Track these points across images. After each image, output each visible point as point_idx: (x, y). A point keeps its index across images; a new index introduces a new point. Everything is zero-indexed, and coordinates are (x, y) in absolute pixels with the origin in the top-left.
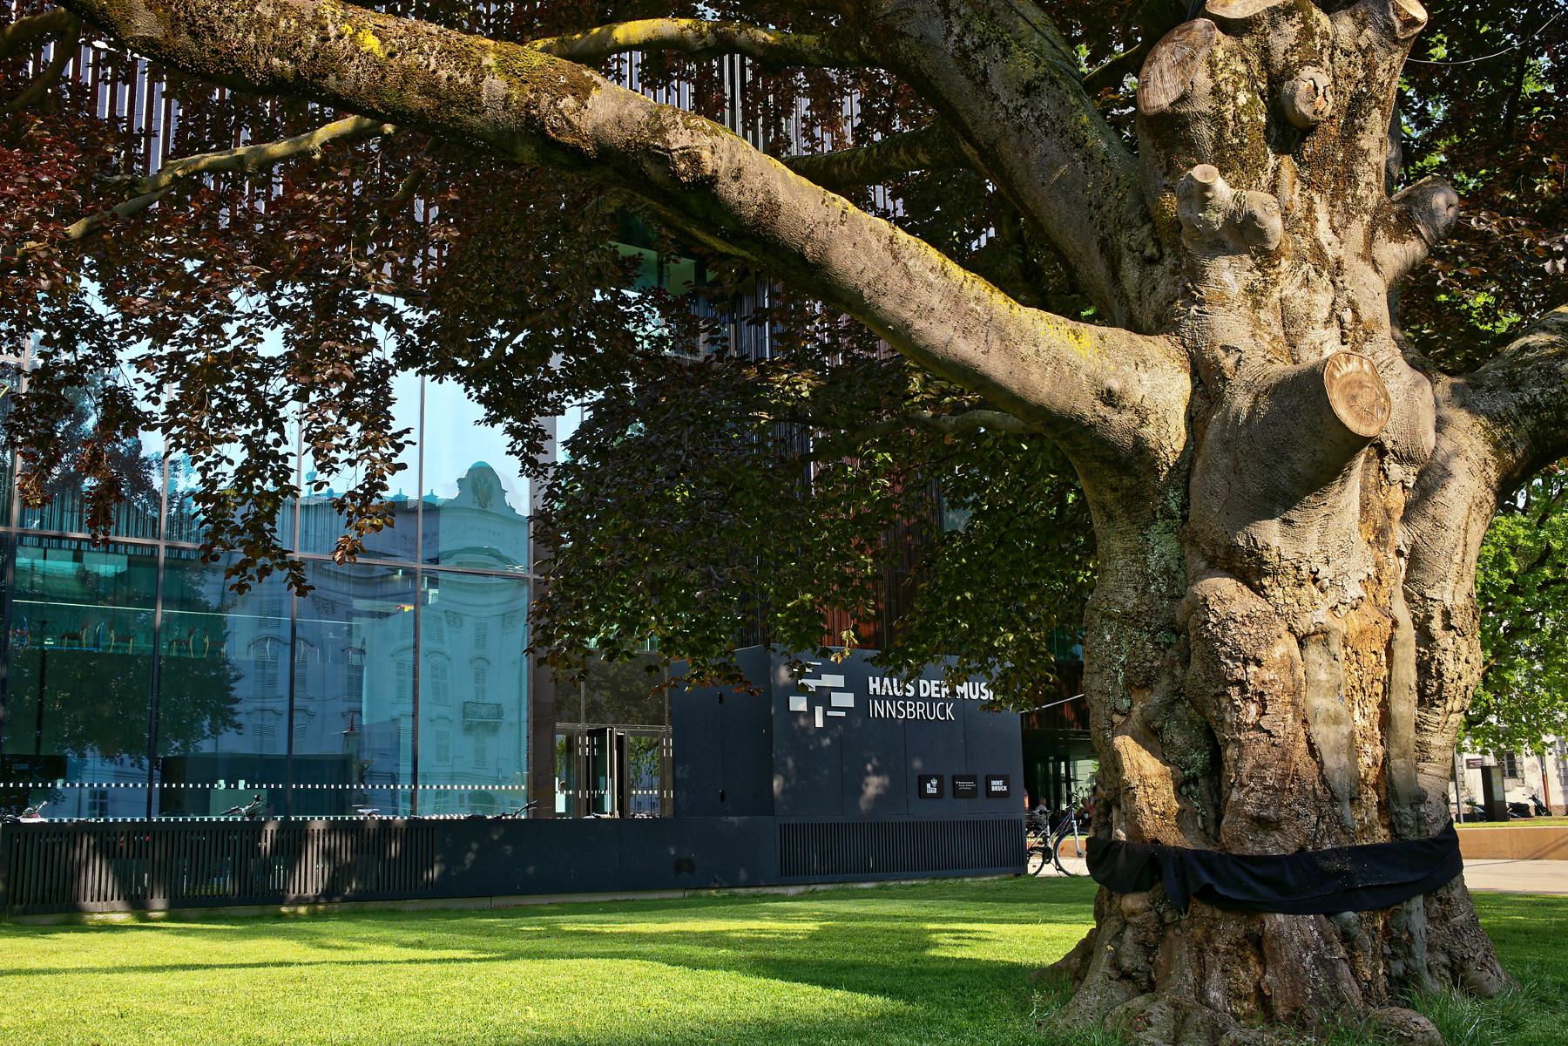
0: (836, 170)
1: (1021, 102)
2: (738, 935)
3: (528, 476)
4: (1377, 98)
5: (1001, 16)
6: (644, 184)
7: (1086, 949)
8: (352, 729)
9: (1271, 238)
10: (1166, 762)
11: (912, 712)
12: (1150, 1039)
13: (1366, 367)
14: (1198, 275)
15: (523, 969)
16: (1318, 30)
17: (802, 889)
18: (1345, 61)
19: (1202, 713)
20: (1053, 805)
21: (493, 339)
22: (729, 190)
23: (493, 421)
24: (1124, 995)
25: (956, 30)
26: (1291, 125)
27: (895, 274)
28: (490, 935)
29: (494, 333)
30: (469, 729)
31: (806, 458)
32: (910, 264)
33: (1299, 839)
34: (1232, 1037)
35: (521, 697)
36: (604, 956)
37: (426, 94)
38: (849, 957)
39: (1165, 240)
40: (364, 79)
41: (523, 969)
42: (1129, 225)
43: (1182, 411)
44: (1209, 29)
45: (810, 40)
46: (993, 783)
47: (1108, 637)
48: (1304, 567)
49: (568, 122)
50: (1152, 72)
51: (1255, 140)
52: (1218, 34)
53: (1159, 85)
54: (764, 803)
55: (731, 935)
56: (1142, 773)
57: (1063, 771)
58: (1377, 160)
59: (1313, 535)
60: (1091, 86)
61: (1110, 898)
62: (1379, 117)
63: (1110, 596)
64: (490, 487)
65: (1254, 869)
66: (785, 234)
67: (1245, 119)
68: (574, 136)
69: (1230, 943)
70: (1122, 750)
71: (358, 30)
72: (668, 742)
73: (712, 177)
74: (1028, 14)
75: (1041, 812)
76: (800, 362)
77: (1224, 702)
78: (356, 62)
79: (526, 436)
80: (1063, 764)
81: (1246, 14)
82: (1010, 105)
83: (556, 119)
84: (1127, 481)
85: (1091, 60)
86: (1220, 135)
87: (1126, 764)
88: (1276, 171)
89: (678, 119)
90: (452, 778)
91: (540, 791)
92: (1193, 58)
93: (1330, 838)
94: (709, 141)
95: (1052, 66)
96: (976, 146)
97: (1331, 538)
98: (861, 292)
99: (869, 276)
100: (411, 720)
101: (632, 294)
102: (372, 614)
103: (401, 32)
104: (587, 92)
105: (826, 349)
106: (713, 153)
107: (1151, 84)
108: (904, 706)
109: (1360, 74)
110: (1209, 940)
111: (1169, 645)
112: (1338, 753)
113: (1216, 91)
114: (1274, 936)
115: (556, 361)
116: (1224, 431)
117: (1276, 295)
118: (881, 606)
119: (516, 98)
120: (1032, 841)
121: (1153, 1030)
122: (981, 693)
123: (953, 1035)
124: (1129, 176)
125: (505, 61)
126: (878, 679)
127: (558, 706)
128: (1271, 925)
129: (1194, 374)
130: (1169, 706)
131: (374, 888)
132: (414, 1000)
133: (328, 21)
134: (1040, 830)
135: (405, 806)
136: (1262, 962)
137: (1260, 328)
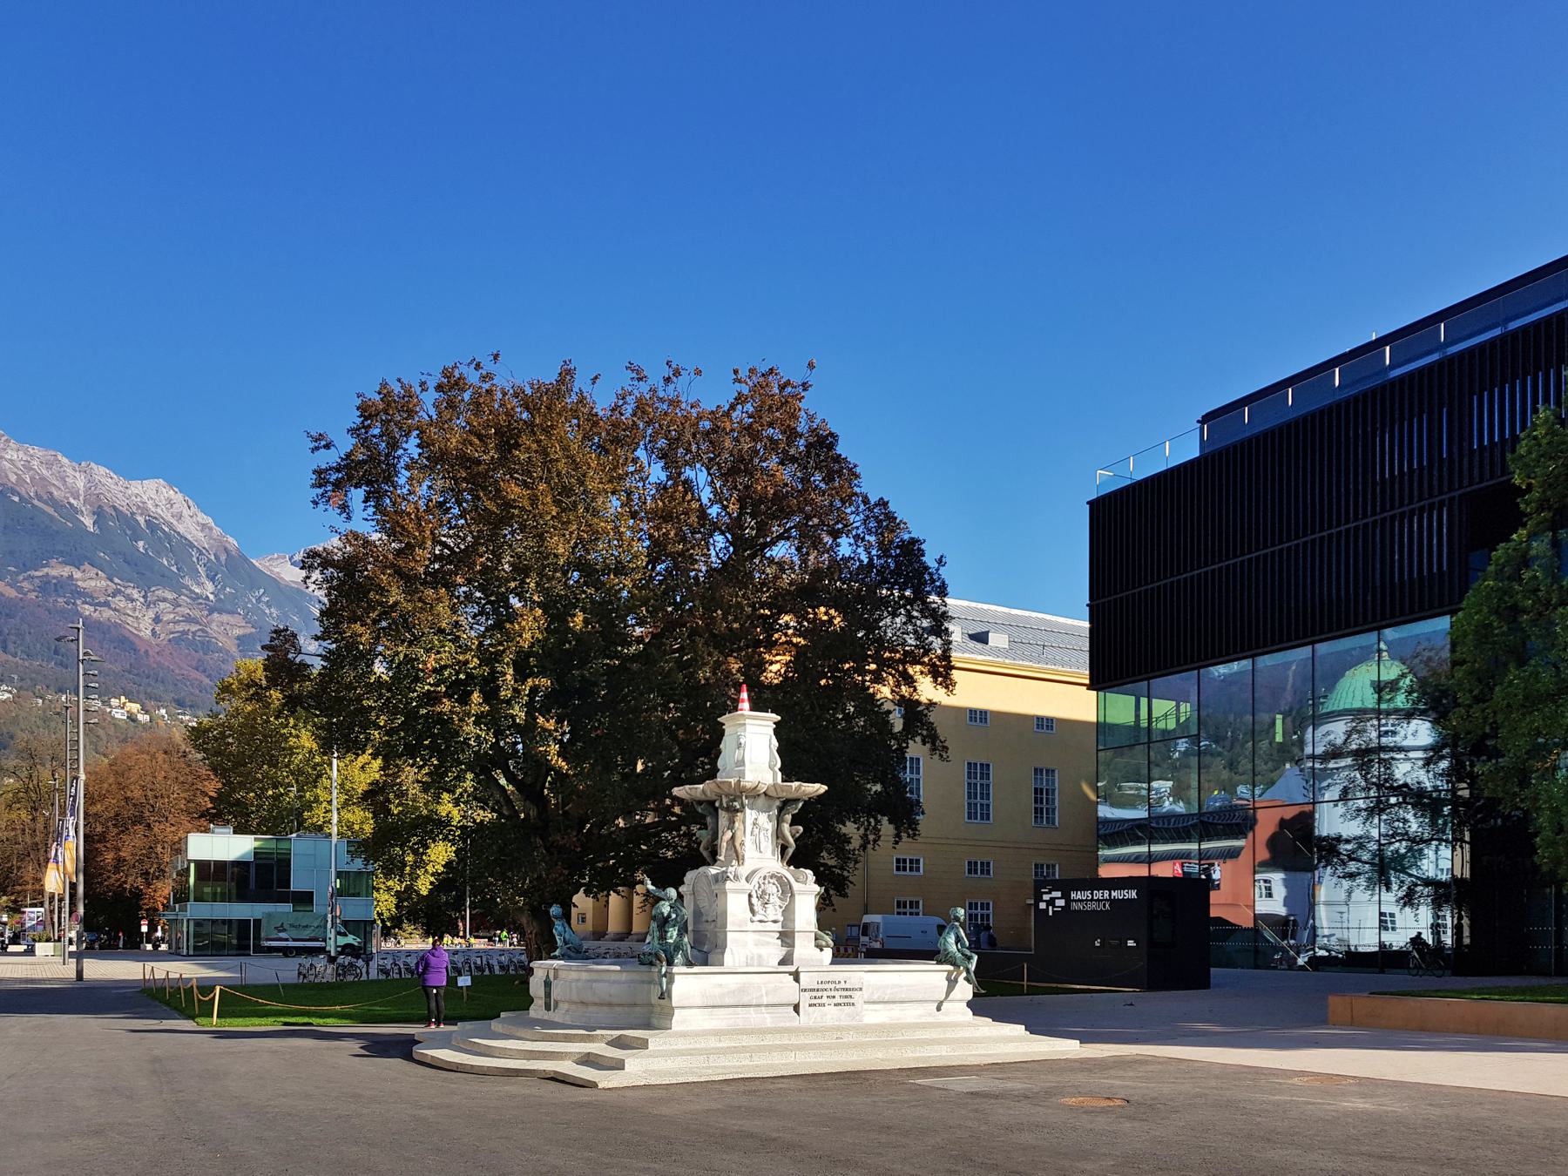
11: (1091, 906)
80: (1467, 941)
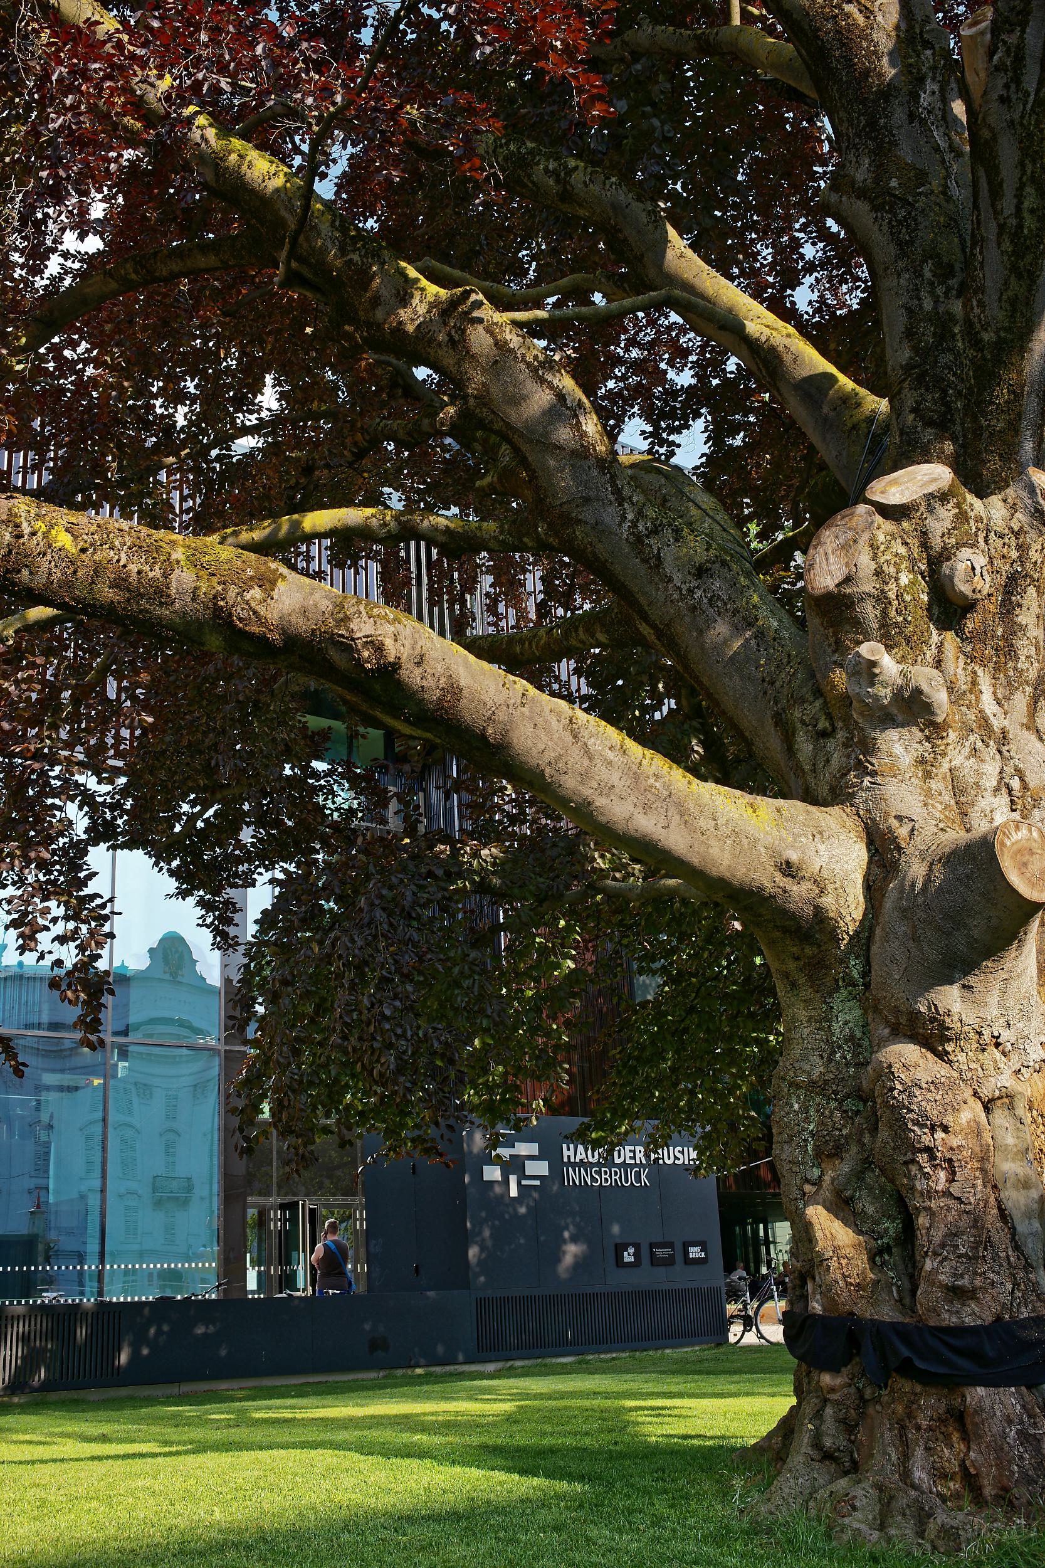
0: (518, 649)
1: (694, 584)
2: (434, 1418)
3: (219, 949)
4: (1031, 577)
5: (674, 502)
6: (329, 671)
7: (788, 1426)
8: (38, 1207)
9: (938, 711)
10: (859, 1232)
11: (606, 1178)
12: (856, 1525)
13: (1035, 834)
14: (868, 747)
15: (210, 1464)
16: (972, 514)
17: (499, 1365)
18: (999, 543)
19: (892, 1181)
20: (752, 1269)
21: (184, 814)
22: (412, 676)
23: (183, 894)
24: (827, 1477)
25: (630, 516)
26: (952, 604)
27: (575, 752)
28: (176, 1426)
29: (185, 808)
30: (158, 1204)
31: (497, 928)
32: (590, 742)
33: (996, 1308)
34: (939, 1521)
35: (211, 1168)
36: (295, 1446)
37: (116, 587)
38: (547, 1441)
39: (836, 714)
40: (57, 574)
41: (210, 1464)
42: (802, 700)
43: (860, 880)
44: (870, 514)
45: (491, 526)
46: (691, 1249)
47: (796, 1106)
48: (986, 1032)
49: (255, 612)
50: (818, 554)
51: (918, 618)
52: (878, 519)
53: (825, 567)
54: (459, 1274)
55: (422, 1418)
56: (835, 1243)
57: (762, 1233)
58: (1035, 634)
59: (993, 999)
60: (762, 564)
61: (808, 1374)
62: (1035, 594)
63: (796, 1065)
64: (181, 957)
65: (951, 1341)
66: (467, 716)
67: (908, 598)
68: (260, 625)
69: (932, 1419)
70: (814, 1220)
71: (52, 527)
72: (361, 1214)
73: (395, 664)
74: (699, 500)
75: (740, 1279)
76: (487, 834)
77: (914, 1169)
78: (49, 557)
79: (218, 909)
80: (761, 1226)
81: (904, 501)
82: (683, 586)
83: (243, 609)
84: (809, 951)
85: (762, 536)
86: (885, 613)
87: (819, 1235)
88: (940, 646)
89: (362, 608)
90: (142, 1256)
91: (232, 1270)
92: (855, 541)
93: (1026, 1306)
94: (391, 629)
95: (722, 549)
96: (653, 626)
97: (1011, 1003)
98: (543, 771)
99: (551, 755)
100: (98, 1196)
101: (320, 766)
102: (61, 1089)
103: (93, 529)
104: (273, 583)
105: (513, 819)
106: (396, 640)
107: (817, 566)
108: (599, 1173)
109: (1014, 555)
110: (910, 1416)
111: (858, 1112)
112: (1030, 1219)
113: (879, 572)
114: (976, 1411)
115: (247, 835)
116: (901, 898)
117: (946, 766)
118: (575, 1070)
119: (204, 590)
120: (732, 1308)
121: (858, 1515)
122: (676, 1158)
123: (654, 1524)
124: (799, 652)
125: (193, 555)
126: (571, 1146)
127: (250, 1178)
128: (973, 1399)
129: (870, 843)
130: (859, 1175)
131: (57, 1375)
132: (95, 1504)
133: (23, 519)
134: (739, 1297)
135: (91, 1286)
136: (966, 1438)
137: (931, 798)
